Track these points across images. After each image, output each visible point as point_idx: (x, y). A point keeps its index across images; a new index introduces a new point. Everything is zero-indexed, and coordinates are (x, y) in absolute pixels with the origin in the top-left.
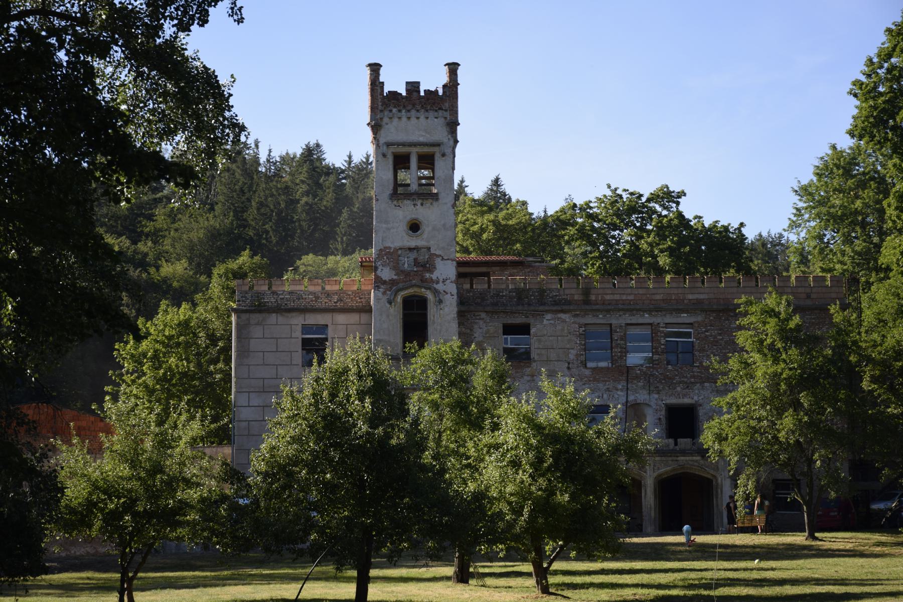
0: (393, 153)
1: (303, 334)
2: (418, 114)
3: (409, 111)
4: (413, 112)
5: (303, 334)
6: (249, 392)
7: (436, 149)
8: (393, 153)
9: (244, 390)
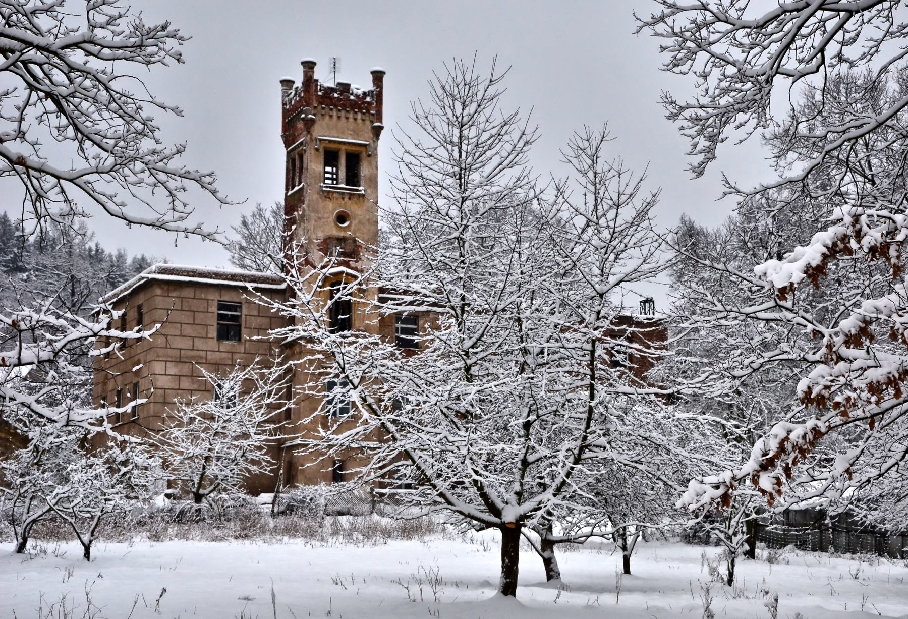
0: (325, 148)
1: (219, 309)
2: (348, 115)
3: (340, 111)
4: (343, 113)
5: (219, 309)
6: (166, 361)
7: (363, 149)
8: (325, 148)
9: (161, 359)
